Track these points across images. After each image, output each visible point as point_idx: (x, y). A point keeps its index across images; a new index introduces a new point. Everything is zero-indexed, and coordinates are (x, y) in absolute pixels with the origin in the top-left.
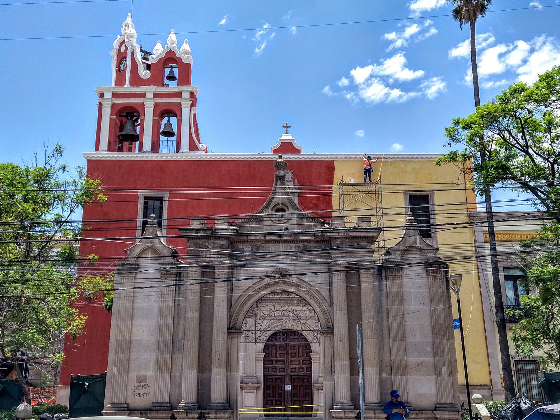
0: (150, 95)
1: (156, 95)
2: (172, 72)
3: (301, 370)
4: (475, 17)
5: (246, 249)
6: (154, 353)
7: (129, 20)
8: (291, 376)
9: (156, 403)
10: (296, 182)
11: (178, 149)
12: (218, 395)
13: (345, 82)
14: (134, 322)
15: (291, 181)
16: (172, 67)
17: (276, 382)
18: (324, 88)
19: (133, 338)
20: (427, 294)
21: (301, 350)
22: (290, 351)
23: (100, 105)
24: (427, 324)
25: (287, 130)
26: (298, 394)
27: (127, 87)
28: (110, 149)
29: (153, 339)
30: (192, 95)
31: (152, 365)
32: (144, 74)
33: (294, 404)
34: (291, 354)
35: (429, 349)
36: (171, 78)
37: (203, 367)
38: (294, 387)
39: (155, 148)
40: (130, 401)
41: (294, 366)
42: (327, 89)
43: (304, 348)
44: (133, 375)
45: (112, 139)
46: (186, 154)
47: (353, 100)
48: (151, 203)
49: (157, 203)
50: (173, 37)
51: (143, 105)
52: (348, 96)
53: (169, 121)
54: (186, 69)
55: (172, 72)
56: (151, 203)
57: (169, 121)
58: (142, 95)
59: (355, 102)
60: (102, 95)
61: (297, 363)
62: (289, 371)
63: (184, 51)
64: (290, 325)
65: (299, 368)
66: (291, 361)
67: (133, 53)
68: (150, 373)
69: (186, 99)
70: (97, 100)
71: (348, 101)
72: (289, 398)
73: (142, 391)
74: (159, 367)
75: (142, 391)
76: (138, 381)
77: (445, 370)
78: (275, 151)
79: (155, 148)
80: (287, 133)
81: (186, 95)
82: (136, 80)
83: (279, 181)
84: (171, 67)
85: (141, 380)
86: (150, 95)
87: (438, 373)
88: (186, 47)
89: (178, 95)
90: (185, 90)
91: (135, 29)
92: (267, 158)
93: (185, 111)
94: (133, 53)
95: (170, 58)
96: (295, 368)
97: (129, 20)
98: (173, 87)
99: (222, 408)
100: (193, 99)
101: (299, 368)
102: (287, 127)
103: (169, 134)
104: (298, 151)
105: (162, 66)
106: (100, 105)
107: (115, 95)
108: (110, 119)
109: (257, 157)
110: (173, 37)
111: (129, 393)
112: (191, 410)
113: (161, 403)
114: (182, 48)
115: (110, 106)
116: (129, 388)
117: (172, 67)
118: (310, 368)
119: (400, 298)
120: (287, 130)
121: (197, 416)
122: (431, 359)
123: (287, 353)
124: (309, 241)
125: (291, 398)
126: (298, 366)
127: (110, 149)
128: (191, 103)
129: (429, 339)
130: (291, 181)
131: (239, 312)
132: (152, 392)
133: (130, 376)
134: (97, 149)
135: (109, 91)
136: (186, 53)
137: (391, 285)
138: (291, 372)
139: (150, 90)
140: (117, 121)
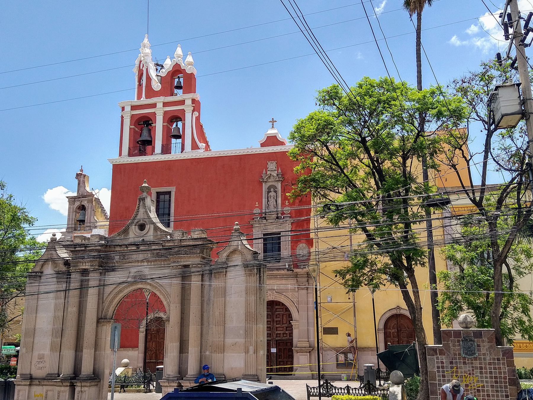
0: (160, 105)
1: (165, 104)
2: (179, 82)
3: (285, 335)
4: (421, 8)
5: (116, 257)
6: (50, 338)
7: (146, 41)
8: (276, 341)
9: (49, 374)
10: (280, 171)
11: (183, 149)
12: (87, 368)
13: (474, 29)
14: (38, 315)
15: (275, 170)
16: (179, 78)
17: (286, 345)
18: (451, 38)
19: (37, 327)
20: (244, 288)
21: (285, 318)
22: (275, 319)
23: (122, 117)
24: (242, 311)
25: (273, 125)
26: (283, 356)
27: (144, 101)
28: (130, 155)
29: (50, 327)
30: (194, 101)
31: (48, 347)
32: (156, 86)
33: (280, 365)
34: (276, 321)
35: (242, 332)
36: (179, 87)
37: (78, 348)
38: (279, 350)
39: (166, 149)
40: (33, 373)
41: (279, 332)
42: (454, 39)
43: (288, 317)
44: (36, 354)
45: (132, 146)
46: (189, 154)
47: (484, 46)
48: (162, 197)
49: (167, 197)
50: (179, 51)
51: (155, 114)
52: (479, 43)
53: (177, 125)
54: (190, 79)
55: (179, 82)
56: (162, 197)
57: (177, 125)
58: (154, 106)
59: (486, 47)
60: (123, 109)
61: (282, 329)
62: (275, 336)
63: (188, 63)
64: (274, 297)
65: (283, 334)
66: (277, 328)
67: (147, 69)
68: (47, 352)
69: (188, 106)
70: (120, 113)
71: (478, 48)
72: (275, 359)
73: (41, 365)
74: (52, 349)
75: (41, 365)
76: (39, 359)
77: (251, 349)
78: (263, 145)
79: (166, 149)
80: (273, 127)
81: (188, 102)
82: (151, 93)
83: (141, 202)
84: (178, 80)
85: (41, 357)
86: (160, 105)
87: (247, 352)
88: (190, 59)
89: (182, 102)
90: (188, 98)
91: (151, 48)
92: (254, 152)
93: (188, 116)
94: (147, 69)
95: (177, 71)
96: (280, 334)
97: (146, 41)
98: (180, 94)
99: (86, 378)
100: (194, 105)
101: (283, 334)
102: (273, 121)
103: (177, 137)
104: (282, 144)
105: (170, 78)
106: (122, 117)
107: (133, 108)
108: (130, 128)
109: (246, 151)
110: (179, 51)
111: (33, 367)
112: (65, 380)
113: (52, 374)
114: (186, 60)
115: (129, 117)
116: (33, 363)
117: (179, 78)
118: (291, 334)
119: (224, 292)
120: (273, 125)
121: (69, 384)
122: (242, 340)
123: (273, 321)
124: (160, 249)
125: (276, 359)
126: (282, 332)
127: (130, 155)
128: (192, 108)
129: (243, 324)
130: (275, 170)
131: (109, 307)
132: (48, 366)
133: (34, 354)
134: (120, 154)
135: (128, 105)
136: (190, 64)
137: (216, 283)
138: (277, 337)
139: (159, 101)
140: (137, 129)
